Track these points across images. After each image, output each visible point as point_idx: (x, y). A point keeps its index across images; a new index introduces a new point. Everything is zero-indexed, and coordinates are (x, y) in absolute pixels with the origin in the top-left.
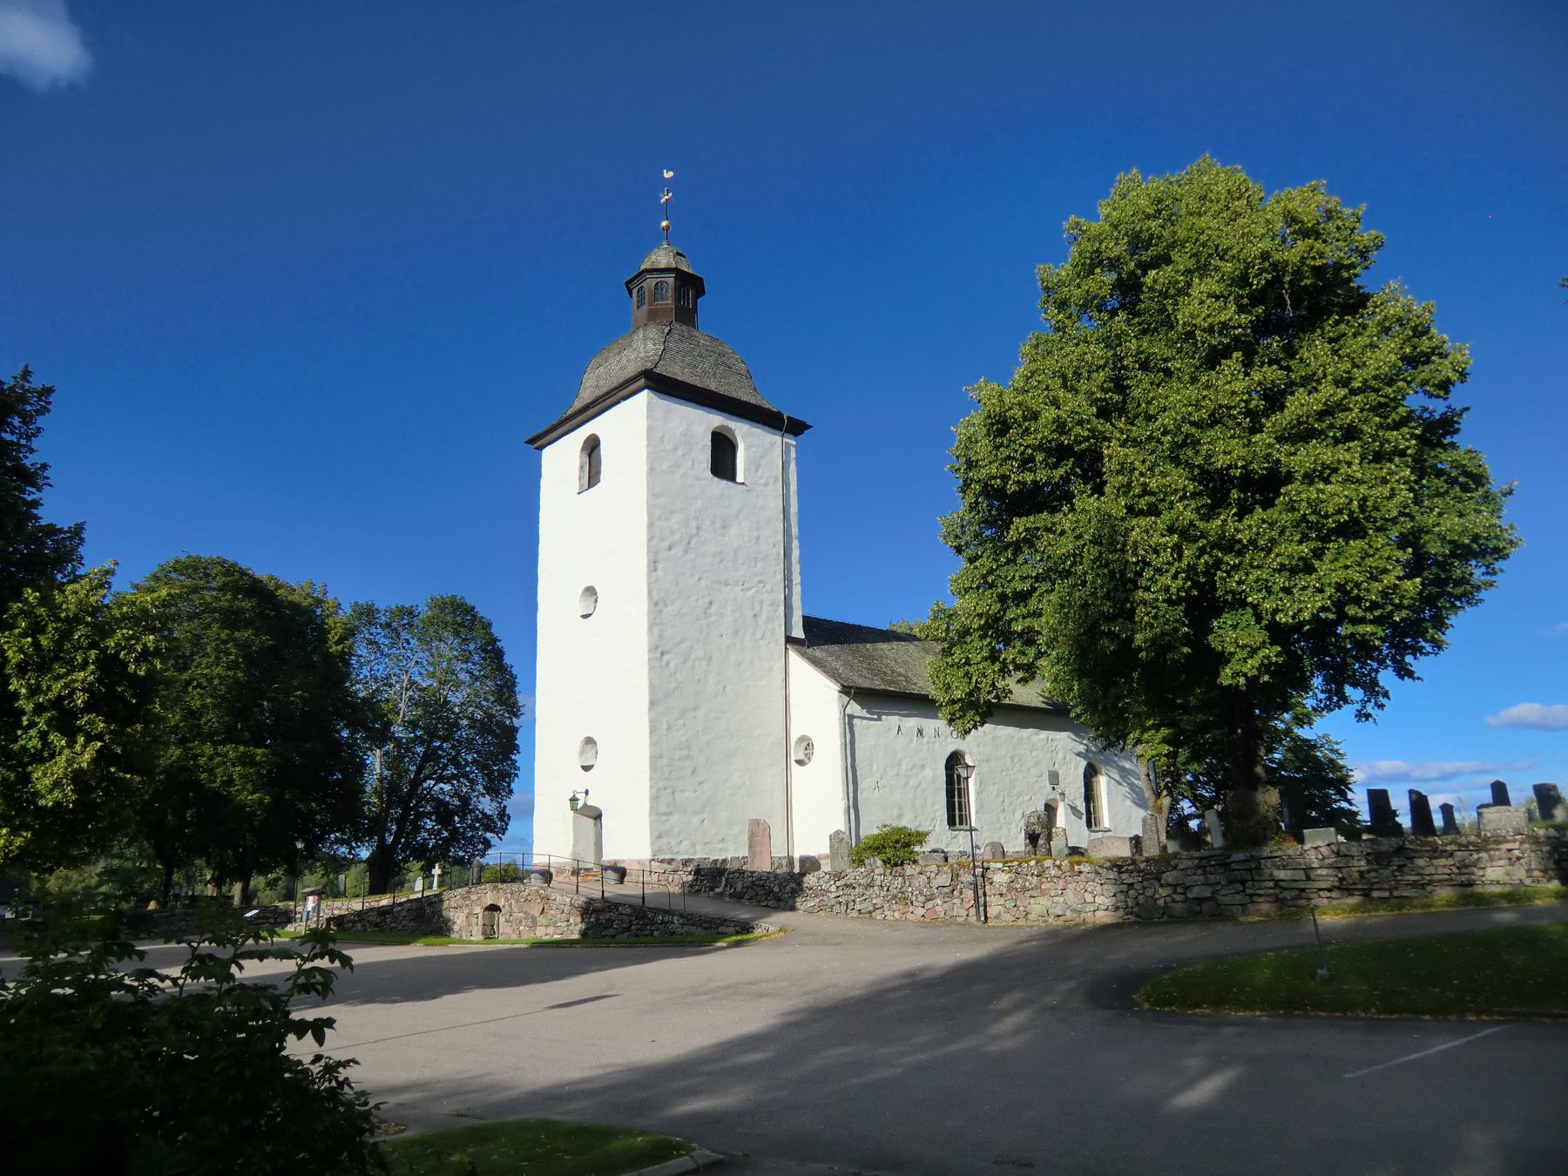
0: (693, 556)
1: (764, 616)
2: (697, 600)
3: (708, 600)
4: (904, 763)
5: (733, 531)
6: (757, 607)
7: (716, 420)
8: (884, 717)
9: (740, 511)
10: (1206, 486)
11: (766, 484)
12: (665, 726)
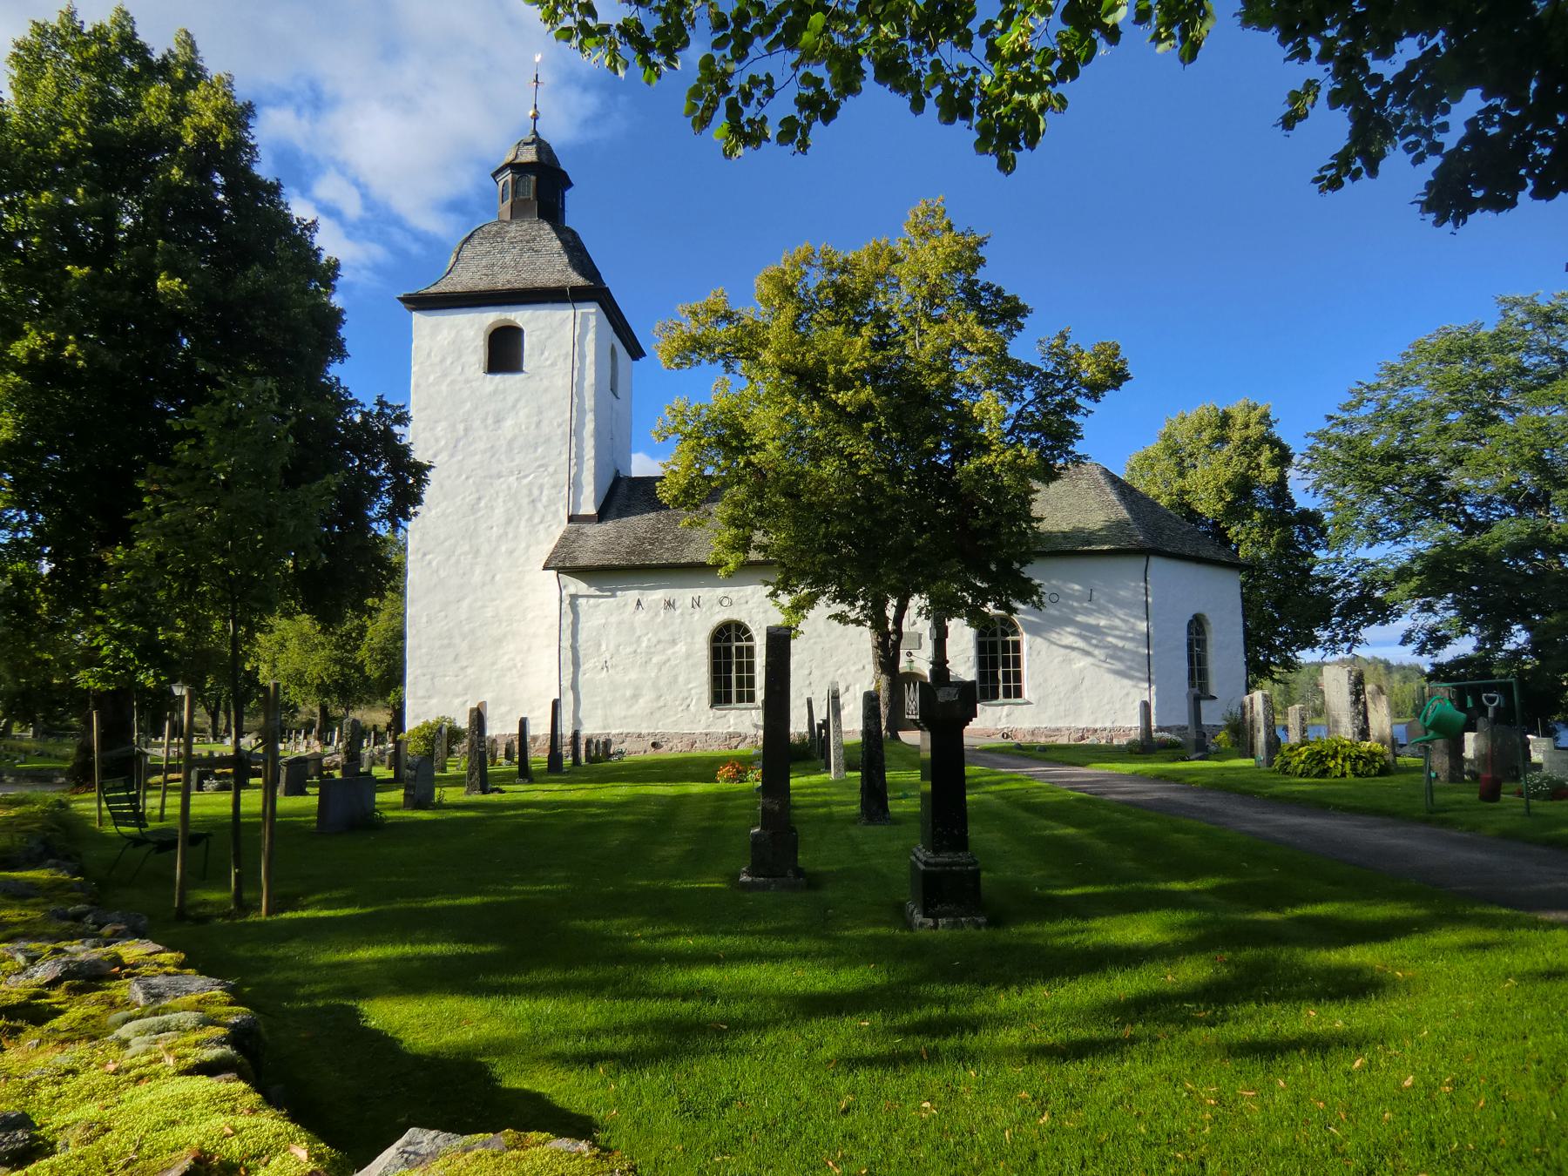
0: (460, 457)
1: (544, 499)
2: (463, 499)
3: (476, 496)
4: (645, 639)
5: (509, 423)
6: (536, 492)
7: (491, 317)
8: (619, 593)
9: (517, 400)
10: (85, 138)
11: (553, 364)
12: (424, 620)
